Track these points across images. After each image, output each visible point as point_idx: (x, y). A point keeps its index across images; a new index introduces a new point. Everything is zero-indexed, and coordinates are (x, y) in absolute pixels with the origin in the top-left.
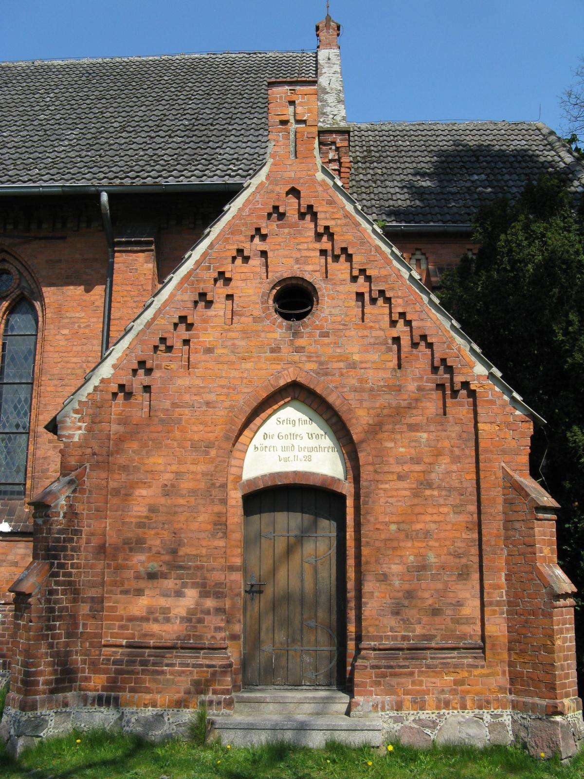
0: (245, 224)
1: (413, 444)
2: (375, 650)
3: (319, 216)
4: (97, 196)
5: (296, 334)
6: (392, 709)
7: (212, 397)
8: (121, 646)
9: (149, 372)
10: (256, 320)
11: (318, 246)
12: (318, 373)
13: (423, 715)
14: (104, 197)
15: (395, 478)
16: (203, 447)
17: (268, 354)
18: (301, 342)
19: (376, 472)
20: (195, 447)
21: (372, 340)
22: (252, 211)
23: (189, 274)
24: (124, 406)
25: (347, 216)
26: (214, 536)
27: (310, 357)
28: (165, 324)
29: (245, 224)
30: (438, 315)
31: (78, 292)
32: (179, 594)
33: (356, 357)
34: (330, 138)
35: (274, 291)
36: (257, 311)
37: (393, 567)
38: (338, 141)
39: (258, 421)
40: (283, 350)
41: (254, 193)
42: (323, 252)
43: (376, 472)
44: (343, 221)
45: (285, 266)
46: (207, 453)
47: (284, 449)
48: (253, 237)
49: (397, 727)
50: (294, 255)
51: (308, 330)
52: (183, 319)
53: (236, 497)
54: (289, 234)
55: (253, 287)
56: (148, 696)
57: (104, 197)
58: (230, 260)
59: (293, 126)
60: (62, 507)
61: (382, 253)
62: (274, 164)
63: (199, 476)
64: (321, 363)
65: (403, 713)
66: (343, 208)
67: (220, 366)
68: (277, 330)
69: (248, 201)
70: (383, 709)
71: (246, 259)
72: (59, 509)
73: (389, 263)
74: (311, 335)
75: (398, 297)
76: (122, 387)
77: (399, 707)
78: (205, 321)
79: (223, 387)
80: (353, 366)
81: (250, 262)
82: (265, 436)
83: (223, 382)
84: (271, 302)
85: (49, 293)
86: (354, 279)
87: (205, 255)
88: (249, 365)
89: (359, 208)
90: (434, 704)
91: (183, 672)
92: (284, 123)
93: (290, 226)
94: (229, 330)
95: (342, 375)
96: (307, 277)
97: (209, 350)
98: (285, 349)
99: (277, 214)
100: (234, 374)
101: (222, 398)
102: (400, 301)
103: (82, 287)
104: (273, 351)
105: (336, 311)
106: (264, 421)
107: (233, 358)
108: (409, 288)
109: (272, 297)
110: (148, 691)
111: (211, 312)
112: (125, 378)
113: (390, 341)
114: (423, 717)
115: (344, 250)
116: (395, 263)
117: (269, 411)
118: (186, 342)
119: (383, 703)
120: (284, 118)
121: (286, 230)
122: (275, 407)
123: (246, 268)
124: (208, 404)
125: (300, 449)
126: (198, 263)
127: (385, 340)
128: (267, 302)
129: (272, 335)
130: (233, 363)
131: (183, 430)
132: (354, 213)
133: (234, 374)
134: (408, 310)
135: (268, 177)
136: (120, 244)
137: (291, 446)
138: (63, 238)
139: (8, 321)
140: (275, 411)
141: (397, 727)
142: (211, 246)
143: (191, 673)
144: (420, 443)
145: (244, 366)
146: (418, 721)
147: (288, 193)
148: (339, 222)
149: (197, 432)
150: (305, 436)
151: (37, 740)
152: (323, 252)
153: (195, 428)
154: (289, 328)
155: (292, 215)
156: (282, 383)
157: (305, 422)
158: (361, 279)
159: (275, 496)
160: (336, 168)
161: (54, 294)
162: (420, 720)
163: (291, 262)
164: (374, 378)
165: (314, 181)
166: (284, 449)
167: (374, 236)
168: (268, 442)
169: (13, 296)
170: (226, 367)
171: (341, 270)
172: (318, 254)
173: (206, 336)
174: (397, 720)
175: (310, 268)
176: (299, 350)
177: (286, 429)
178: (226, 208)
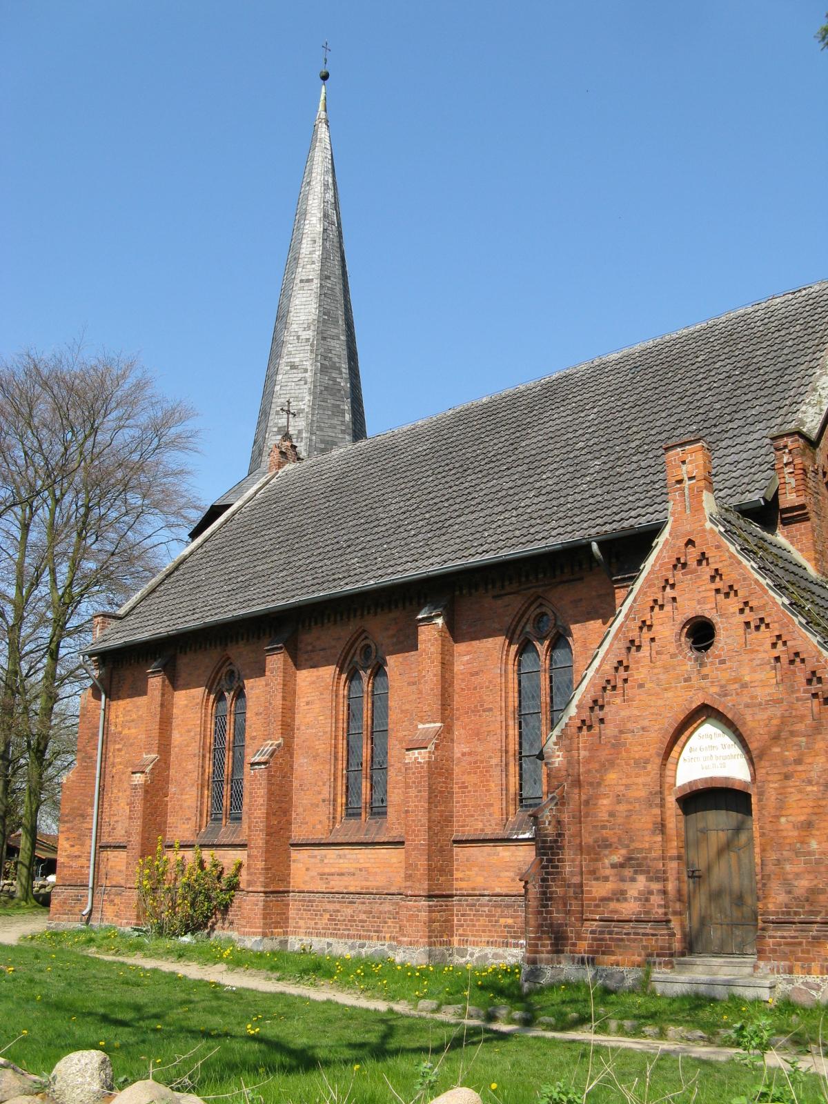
0: (657, 578)
1: (795, 748)
2: (773, 923)
3: (710, 561)
4: (589, 545)
5: (702, 665)
6: (785, 972)
7: (646, 723)
8: (596, 920)
9: (602, 707)
10: (673, 656)
11: (714, 586)
12: (719, 695)
13: (810, 979)
14: (595, 546)
15: (576, 791)
16: (642, 763)
17: (683, 684)
18: (705, 671)
19: (767, 774)
20: (637, 762)
21: (758, 662)
22: (662, 565)
23: (622, 626)
24: (588, 736)
25: (732, 556)
26: (653, 833)
27: (712, 682)
28: (608, 667)
29: (657, 578)
30: (808, 634)
31: (598, 625)
32: (633, 880)
33: (747, 678)
34: (781, 443)
35: (686, 630)
36: (672, 649)
37: (784, 853)
38: (789, 444)
39: (683, 738)
40: (693, 679)
41: (661, 551)
42: (718, 591)
43: (767, 774)
44: (729, 561)
45: (690, 607)
46: (645, 768)
47: (705, 759)
48: (664, 588)
49: (790, 987)
50: (695, 599)
51: (710, 660)
52: (620, 663)
53: (671, 800)
54: (691, 579)
55: (668, 628)
56: (613, 958)
57: (595, 546)
58: (649, 609)
59: (687, 483)
60: (547, 817)
61: (760, 585)
62: (674, 521)
63: (641, 787)
64: (722, 687)
65: (795, 976)
66: (728, 550)
67: (650, 698)
68: (687, 660)
69: (658, 558)
70: (778, 972)
71: (662, 607)
72: (544, 819)
73: (766, 592)
74: (712, 663)
75: (775, 622)
76: (583, 721)
77: (791, 972)
78: (637, 662)
79: (652, 714)
80: (744, 686)
81: (665, 608)
82: (691, 750)
83: (654, 710)
84: (683, 639)
85: (575, 628)
86: (742, 611)
87: (631, 608)
88: (669, 694)
89: (739, 548)
90: (818, 969)
91: (636, 939)
92: (680, 482)
93: (692, 572)
94: (654, 668)
95: (737, 694)
96: (707, 615)
97: (641, 686)
98: (694, 676)
99: (680, 565)
100: (660, 702)
101: (653, 723)
102: (776, 625)
103: (600, 621)
104: (686, 680)
105: (729, 641)
106: (688, 738)
107: (657, 689)
108: (783, 612)
109: (684, 634)
110: (613, 953)
111: (640, 654)
112: (585, 715)
113: (772, 661)
114: (809, 980)
115: (731, 587)
116: (770, 592)
117: (691, 729)
118: (626, 681)
119: (778, 967)
120: (678, 478)
121: (689, 577)
122: (695, 725)
123: (662, 614)
124: (643, 729)
125: (717, 758)
126: (627, 616)
127: (769, 660)
128: (680, 640)
129: (684, 668)
130: (658, 694)
131: (628, 751)
132: (736, 554)
133: (660, 702)
134: (784, 632)
135: (670, 534)
136: (617, 581)
137: (710, 757)
138: (581, 579)
139: (551, 656)
140: (696, 729)
141: (790, 987)
142: (635, 600)
143: (641, 940)
144: (800, 746)
145: (666, 695)
146: (806, 983)
147: (687, 545)
148: (725, 563)
149: (637, 752)
150: (720, 747)
151: (538, 985)
152: (718, 591)
153: (636, 749)
154: (696, 660)
155: (693, 564)
156: (694, 706)
157: (719, 735)
158: (747, 610)
159: (700, 799)
160: (791, 470)
161: (580, 630)
162: (807, 982)
163: (695, 603)
164: (762, 694)
165: (704, 530)
166: (705, 759)
167: (753, 571)
168: (693, 755)
169: (552, 635)
170: (654, 698)
171: (733, 604)
172: (714, 593)
173: (639, 673)
174: (790, 982)
175: (708, 606)
176: (705, 677)
177: (706, 742)
178: (641, 567)
